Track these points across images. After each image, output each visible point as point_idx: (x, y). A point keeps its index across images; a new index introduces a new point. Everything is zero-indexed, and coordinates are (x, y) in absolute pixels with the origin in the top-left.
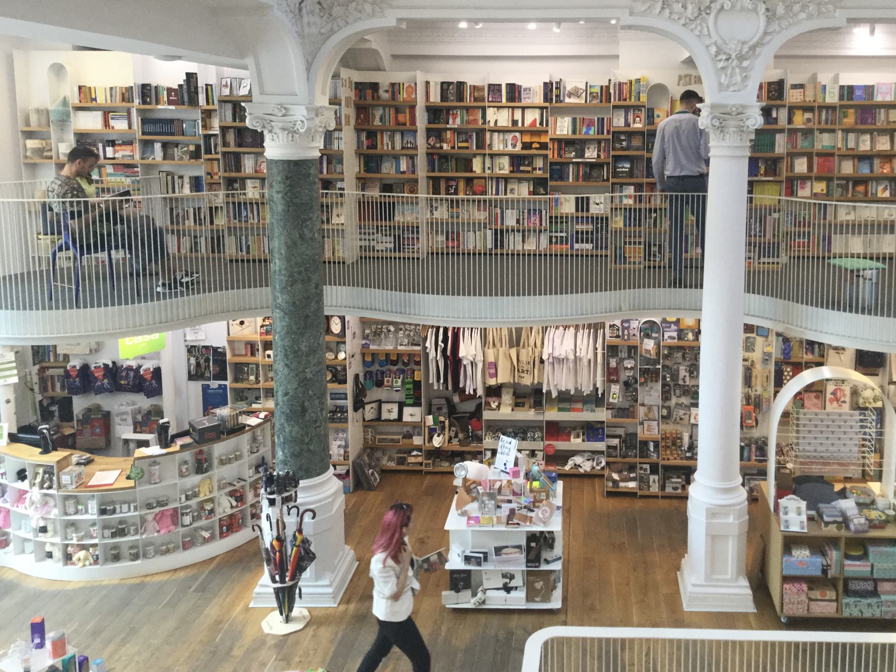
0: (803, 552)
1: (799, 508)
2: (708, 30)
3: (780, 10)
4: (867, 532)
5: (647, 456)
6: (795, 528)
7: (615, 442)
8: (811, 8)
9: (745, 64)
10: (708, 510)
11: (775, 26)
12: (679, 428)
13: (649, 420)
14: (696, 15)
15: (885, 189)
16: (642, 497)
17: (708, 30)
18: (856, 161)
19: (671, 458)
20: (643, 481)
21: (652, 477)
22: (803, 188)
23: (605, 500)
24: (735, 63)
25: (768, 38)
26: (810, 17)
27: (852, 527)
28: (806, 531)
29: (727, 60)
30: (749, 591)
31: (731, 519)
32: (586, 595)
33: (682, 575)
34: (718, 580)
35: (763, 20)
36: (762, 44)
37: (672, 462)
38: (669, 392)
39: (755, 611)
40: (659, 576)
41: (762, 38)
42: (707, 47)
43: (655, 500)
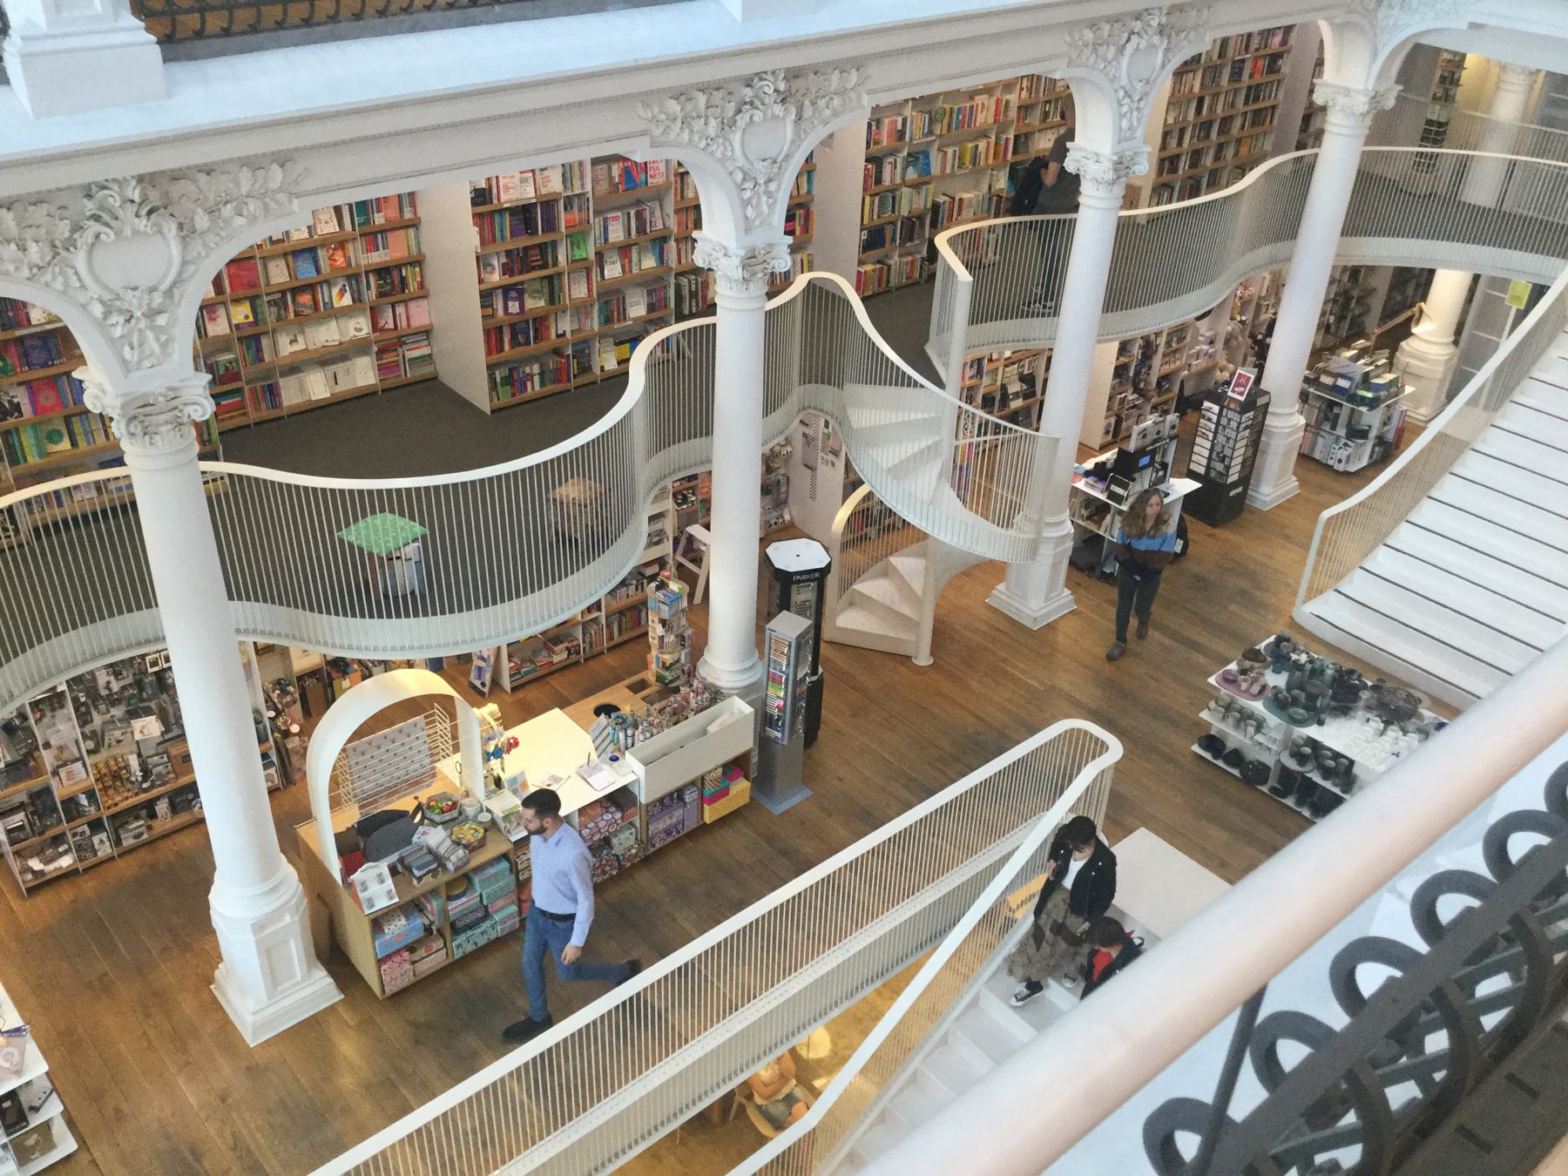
0: (399, 923)
1: (380, 875)
2: (80, 279)
3: (202, 221)
4: (468, 862)
5: (80, 814)
6: (382, 903)
7: (18, 819)
8: (252, 208)
9: (161, 320)
10: (253, 926)
11: (197, 246)
12: (116, 751)
13: (65, 764)
14: (48, 258)
15: (342, 292)
16: (86, 870)
17: (80, 279)
18: (290, 258)
19: (118, 798)
20: (84, 849)
21: (96, 840)
22: (213, 319)
23: (28, 904)
24: (143, 324)
25: (191, 268)
26: (253, 219)
27: (450, 866)
28: (397, 900)
29: (128, 321)
30: (330, 980)
31: (288, 919)
32: (97, 1098)
33: (219, 987)
34: (288, 989)
35: (175, 248)
36: (182, 281)
37: (124, 805)
38: (88, 712)
39: (342, 996)
40: (187, 1006)
41: (180, 273)
42: (84, 307)
43: (112, 864)
